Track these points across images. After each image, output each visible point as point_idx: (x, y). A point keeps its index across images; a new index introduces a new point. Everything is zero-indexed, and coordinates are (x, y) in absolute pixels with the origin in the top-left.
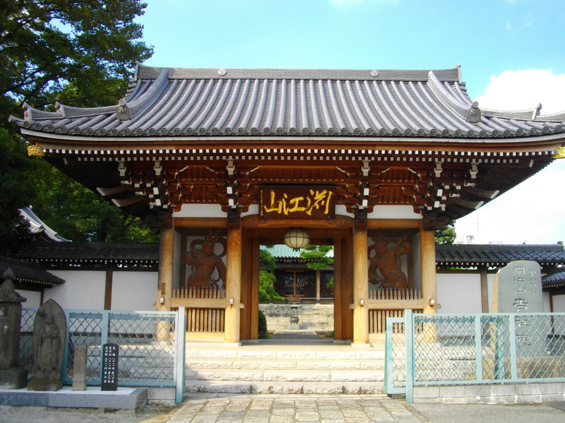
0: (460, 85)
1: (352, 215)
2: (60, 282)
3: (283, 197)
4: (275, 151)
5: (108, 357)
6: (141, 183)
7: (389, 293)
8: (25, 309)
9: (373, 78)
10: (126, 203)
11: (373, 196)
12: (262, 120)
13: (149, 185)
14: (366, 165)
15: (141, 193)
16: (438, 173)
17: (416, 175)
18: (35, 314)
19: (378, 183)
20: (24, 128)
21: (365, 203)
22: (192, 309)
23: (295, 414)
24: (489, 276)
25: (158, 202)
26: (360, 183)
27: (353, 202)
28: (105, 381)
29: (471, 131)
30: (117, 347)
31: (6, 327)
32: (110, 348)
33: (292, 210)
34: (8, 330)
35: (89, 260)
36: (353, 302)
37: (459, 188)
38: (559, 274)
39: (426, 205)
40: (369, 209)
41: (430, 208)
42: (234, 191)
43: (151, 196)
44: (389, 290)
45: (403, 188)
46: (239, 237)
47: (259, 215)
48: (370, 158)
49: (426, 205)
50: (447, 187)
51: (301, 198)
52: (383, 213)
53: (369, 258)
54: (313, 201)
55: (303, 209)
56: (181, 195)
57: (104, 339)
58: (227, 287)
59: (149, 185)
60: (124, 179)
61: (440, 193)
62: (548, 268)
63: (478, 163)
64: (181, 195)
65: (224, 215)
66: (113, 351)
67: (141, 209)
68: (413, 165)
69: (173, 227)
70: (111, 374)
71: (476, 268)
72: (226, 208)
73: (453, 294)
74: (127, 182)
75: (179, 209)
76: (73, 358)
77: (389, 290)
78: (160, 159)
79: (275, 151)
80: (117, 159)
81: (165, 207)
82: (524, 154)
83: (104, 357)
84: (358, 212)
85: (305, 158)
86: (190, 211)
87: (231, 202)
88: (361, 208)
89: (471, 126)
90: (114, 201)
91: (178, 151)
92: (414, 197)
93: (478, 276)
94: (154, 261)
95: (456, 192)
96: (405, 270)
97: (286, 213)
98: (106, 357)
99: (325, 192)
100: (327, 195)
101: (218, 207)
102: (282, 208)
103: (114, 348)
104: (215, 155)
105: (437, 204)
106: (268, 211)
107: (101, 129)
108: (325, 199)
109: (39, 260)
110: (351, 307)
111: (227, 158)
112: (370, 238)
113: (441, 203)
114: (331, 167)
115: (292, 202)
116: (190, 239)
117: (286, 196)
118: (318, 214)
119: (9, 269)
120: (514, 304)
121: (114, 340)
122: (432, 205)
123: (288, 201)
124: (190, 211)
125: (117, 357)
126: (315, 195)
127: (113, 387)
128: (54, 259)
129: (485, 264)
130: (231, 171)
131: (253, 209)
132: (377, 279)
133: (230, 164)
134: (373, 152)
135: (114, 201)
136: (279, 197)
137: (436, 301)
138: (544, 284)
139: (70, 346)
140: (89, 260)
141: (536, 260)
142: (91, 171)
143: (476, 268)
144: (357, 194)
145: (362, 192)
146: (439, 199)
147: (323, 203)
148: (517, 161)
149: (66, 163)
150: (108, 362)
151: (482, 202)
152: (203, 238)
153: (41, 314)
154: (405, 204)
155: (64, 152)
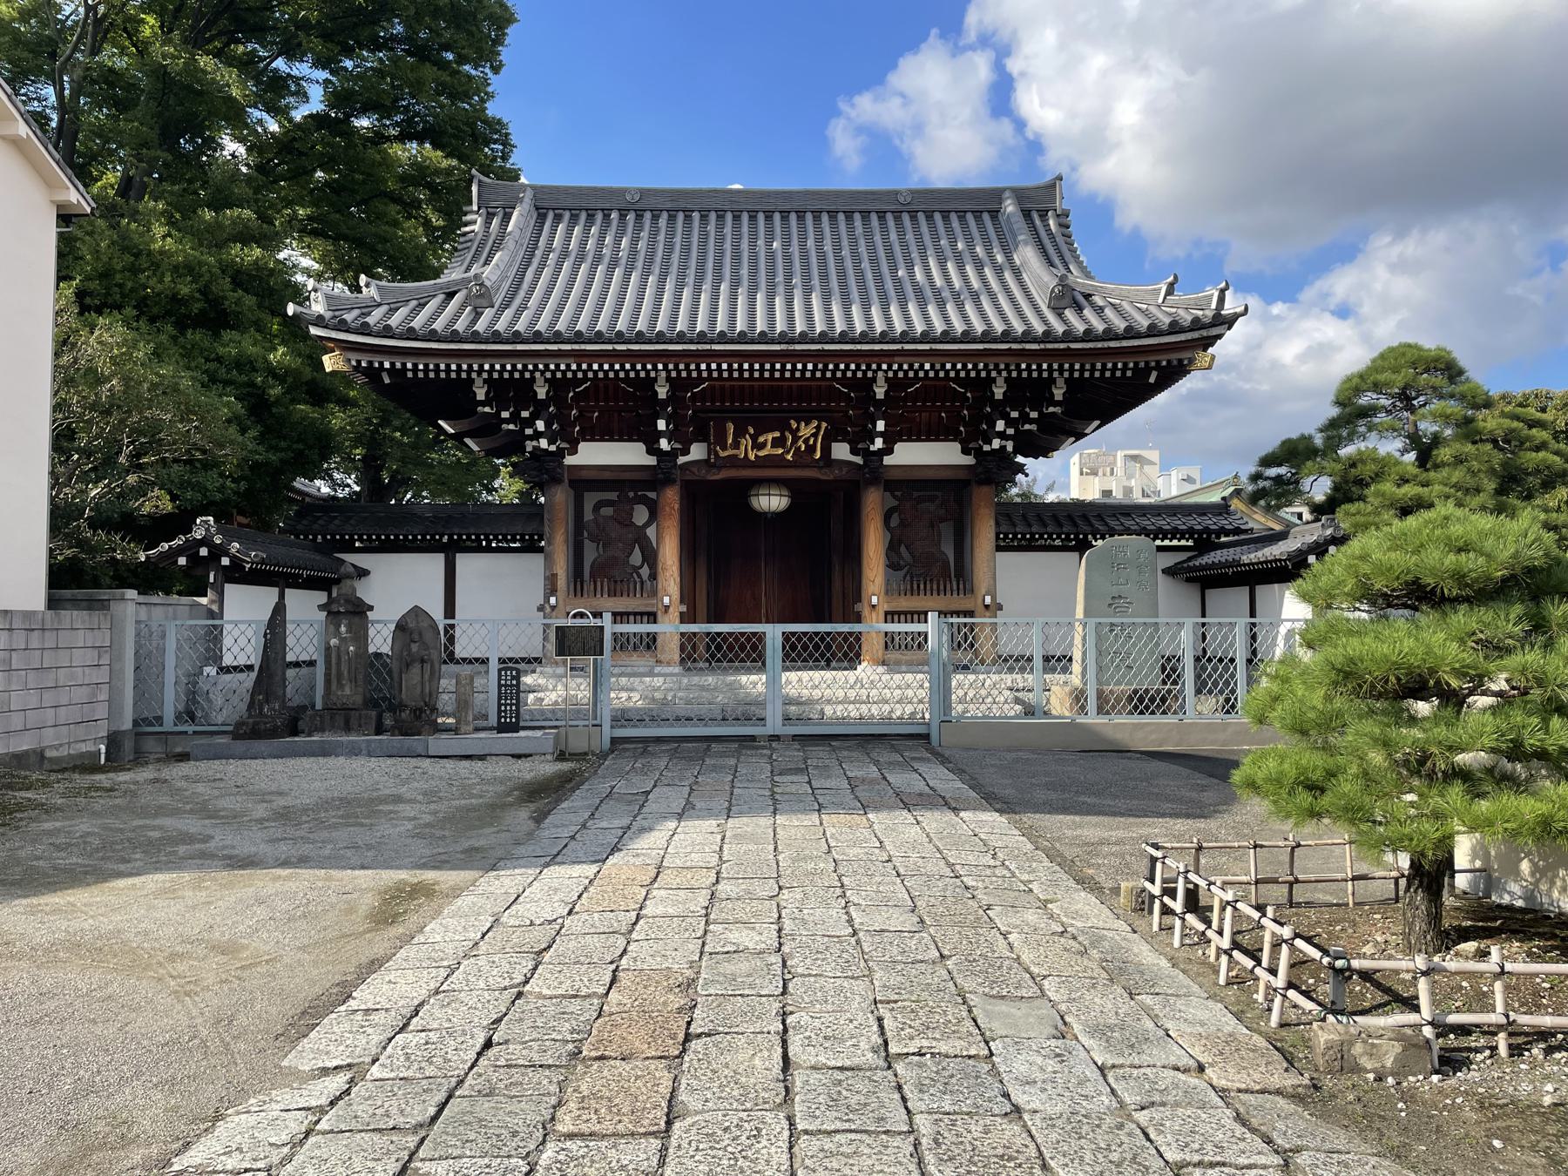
1: (858, 460)
3: (747, 431)
9: (900, 208)
12: (595, 318)
13: (525, 414)
15: (511, 427)
16: (999, 392)
21: (879, 443)
27: (861, 439)
33: (761, 453)
37: (1034, 415)
40: (888, 450)
43: (529, 431)
47: (707, 461)
50: (1015, 414)
51: (777, 434)
52: (908, 454)
54: (796, 439)
55: (780, 451)
58: (660, 578)
59: (525, 414)
60: (483, 404)
65: (651, 461)
66: (513, 678)
72: (652, 450)
73: (1020, 582)
74: (487, 409)
75: (574, 451)
84: (867, 454)
86: (593, 454)
88: (872, 448)
90: (468, 441)
95: (1031, 421)
97: (752, 458)
100: (818, 428)
101: (641, 447)
106: (723, 454)
108: (815, 435)
110: (857, 607)
115: (761, 439)
116: (590, 500)
117: (752, 431)
123: (754, 438)
124: (593, 454)
126: (798, 429)
127: (515, 728)
130: (662, 392)
131: (697, 452)
135: (468, 441)
136: (740, 433)
137: (994, 598)
152: (613, 496)
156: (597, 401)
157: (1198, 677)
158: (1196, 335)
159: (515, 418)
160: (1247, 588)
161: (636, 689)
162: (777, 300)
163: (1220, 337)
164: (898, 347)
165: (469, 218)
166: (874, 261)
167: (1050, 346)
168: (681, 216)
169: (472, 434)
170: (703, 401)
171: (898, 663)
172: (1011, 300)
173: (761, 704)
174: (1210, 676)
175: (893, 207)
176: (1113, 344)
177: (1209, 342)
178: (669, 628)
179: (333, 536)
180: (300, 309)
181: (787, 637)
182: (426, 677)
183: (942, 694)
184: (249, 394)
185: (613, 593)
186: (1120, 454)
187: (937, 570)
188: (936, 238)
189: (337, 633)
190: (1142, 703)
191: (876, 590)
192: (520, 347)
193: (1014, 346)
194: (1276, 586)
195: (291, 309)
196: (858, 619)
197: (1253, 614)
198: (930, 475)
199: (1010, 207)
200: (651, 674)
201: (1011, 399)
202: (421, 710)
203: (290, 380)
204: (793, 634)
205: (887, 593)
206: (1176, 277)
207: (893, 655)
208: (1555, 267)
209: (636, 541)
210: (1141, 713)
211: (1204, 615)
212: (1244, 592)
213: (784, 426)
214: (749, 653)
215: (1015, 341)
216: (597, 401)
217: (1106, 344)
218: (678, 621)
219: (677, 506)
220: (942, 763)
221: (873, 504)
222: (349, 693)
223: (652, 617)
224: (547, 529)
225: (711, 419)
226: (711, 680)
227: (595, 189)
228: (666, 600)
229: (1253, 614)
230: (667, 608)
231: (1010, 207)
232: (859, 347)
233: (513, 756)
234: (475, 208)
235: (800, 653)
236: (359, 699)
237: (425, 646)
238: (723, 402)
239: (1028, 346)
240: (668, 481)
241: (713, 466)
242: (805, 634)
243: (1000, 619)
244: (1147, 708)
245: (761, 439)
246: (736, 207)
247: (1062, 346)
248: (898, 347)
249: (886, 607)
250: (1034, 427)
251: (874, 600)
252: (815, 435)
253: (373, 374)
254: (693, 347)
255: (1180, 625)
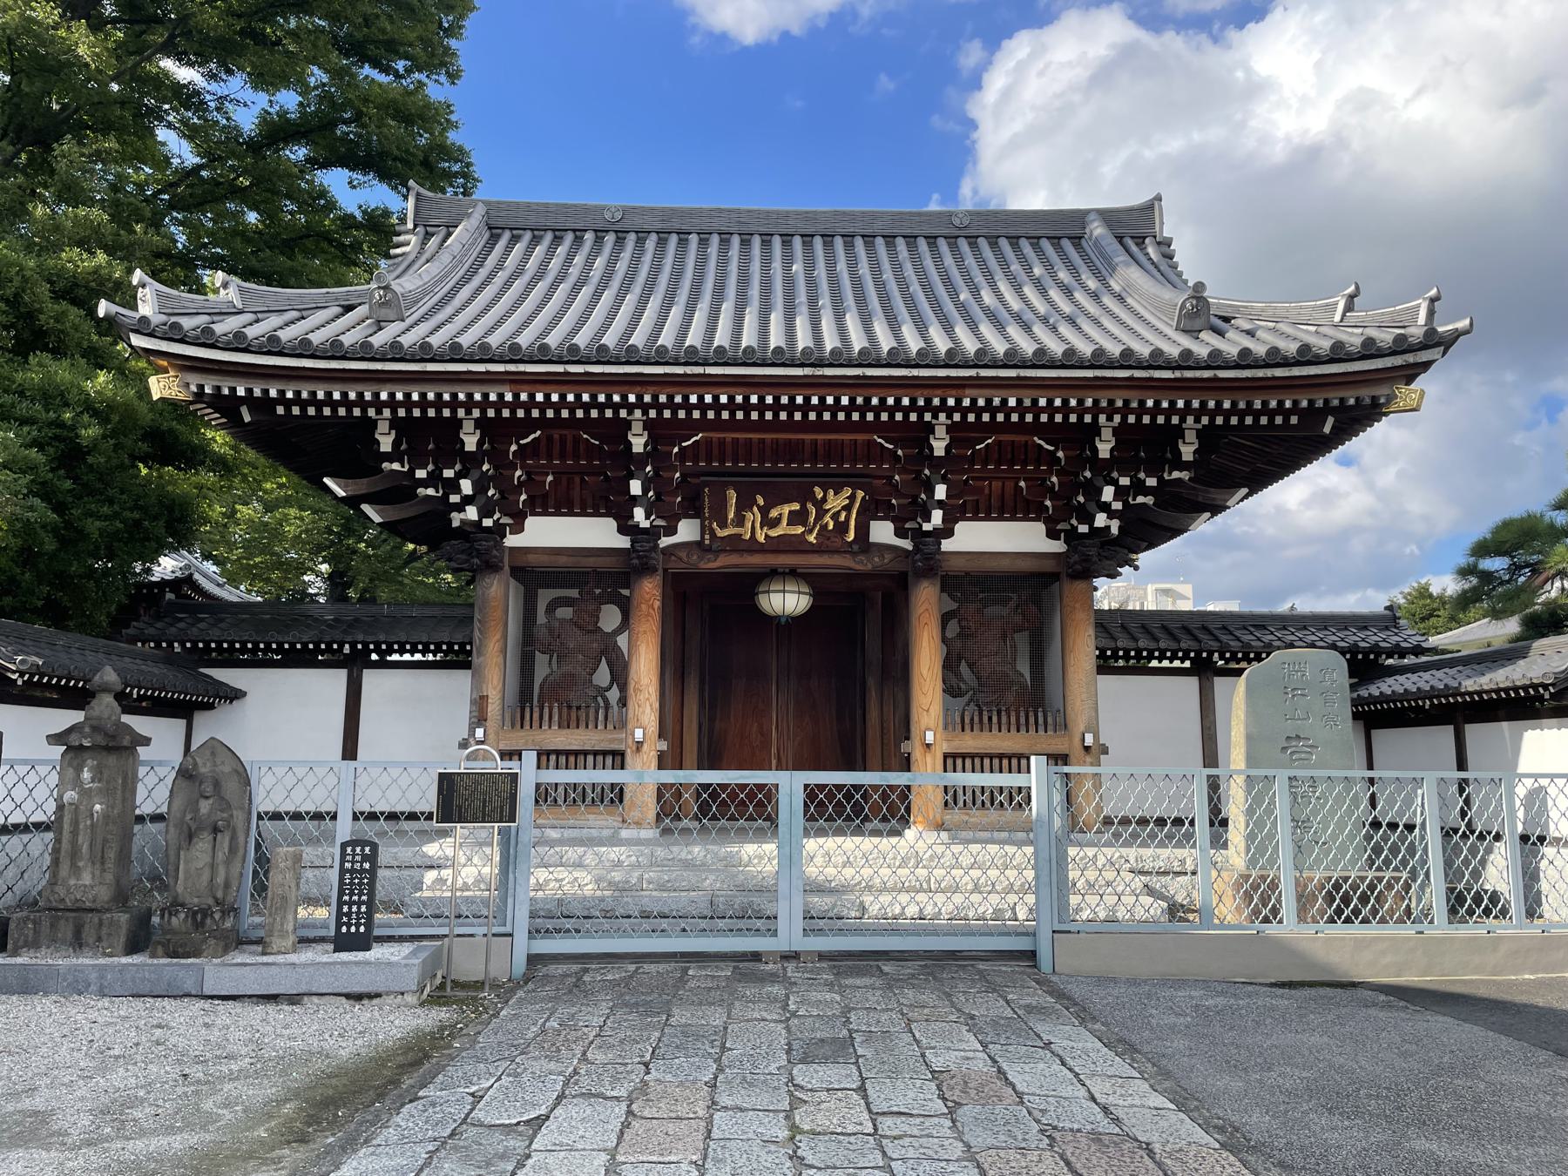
0: (1159, 243)
1: (906, 544)
2: (235, 695)
3: (755, 502)
4: (739, 399)
5: (352, 871)
6: (430, 467)
7: (990, 719)
8: (145, 763)
9: (958, 233)
10: (396, 513)
11: (953, 502)
13: (448, 473)
14: (940, 431)
15: (431, 492)
16: (1104, 449)
17: (1053, 453)
18: (174, 774)
19: (964, 472)
20: (137, 332)
21: (937, 517)
22: (548, 753)
23: (787, 997)
24: (1219, 682)
25: (472, 513)
26: (927, 472)
27: (907, 515)
28: (344, 929)
29: (1187, 353)
30: (374, 847)
31: (98, 807)
32: (358, 850)
33: (774, 533)
34: (106, 816)
35: (305, 645)
36: (908, 738)
37: (1151, 482)
38: (1390, 681)
39: (1074, 521)
40: (947, 532)
41: (1083, 529)
42: (645, 490)
43: (454, 499)
44: (990, 711)
45: (1022, 484)
46: (657, 593)
47: (699, 544)
48: (949, 417)
49: (1074, 521)
50: (1125, 481)
51: (796, 506)
52: (977, 538)
53: (944, 640)
54: (821, 513)
55: (800, 530)
56: (523, 497)
57: (344, 829)
58: (630, 704)
59: (448, 473)
60: (389, 457)
61: (1108, 493)
62: (1364, 666)
63: (1199, 426)
64: (523, 497)
65: (623, 542)
66: (365, 858)
67: (432, 527)
68: (1049, 431)
69: (507, 568)
70: (358, 913)
71: (1187, 664)
72: (626, 527)
73: (1134, 718)
74: (396, 466)
75: (518, 528)
76: (266, 873)
77: (990, 711)
78: (476, 413)
79: (739, 399)
80: (371, 412)
81: (488, 522)
82: (1311, 402)
83: (343, 871)
84: (918, 535)
85: (805, 416)
86: (545, 532)
87: (639, 514)
88: (927, 527)
89: (1186, 342)
90: (366, 508)
91: (516, 396)
92: (1048, 503)
93: (1193, 682)
94: (462, 645)
95: (1147, 491)
96: (1024, 668)
97: (761, 539)
98: (348, 871)
99: (848, 492)
100: (852, 498)
101: (611, 523)
102: (753, 527)
103: (367, 850)
104: (601, 408)
105: (1101, 520)
106: (721, 533)
107: (336, 343)
108: (848, 508)
109: (183, 645)
110: (905, 747)
111: (630, 413)
112: (945, 595)
113: (1110, 517)
114: (860, 437)
115: (774, 513)
116: (545, 597)
117: (761, 501)
118: (831, 541)
119: (108, 669)
120: (1284, 749)
121: (369, 829)
122: (1090, 520)
123: (764, 511)
124: (545, 532)
125: (374, 867)
126: (824, 500)
127: (362, 942)
128: (219, 644)
129: (1211, 654)
130: (638, 443)
131: (687, 531)
132: (963, 686)
133: (637, 427)
134: (959, 401)
135: (366, 508)
136: (745, 504)
137: (1096, 738)
138: (1356, 702)
139: (258, 846)
140: (305, 645)
141: (1333, 647)
142: (307, 436)
143: (1187, 664)
144: (918, 496)
145: (931, 492)
146: (1105, 507)
147: (842, 518)
148: (1294, 420)
149: (247, 418)
150: (351, 884)
151: (1208, 515)
152: (574, 593)
153: (186, 774)
154: (1026, 519)
155: (241, 392)
156: (550, 458)
157: (1448, 863)
158: (1398, 361)
159: (434, 479)
160: (1451, 728)
161: (576, 866)
162: (798, 321)
163: (1426, 365)
164: (971, 373)
165: (401, 238)
166: (927, 287)
167: (1189, 374)
168: (674, 239)
169: (371, 499)
170: (696, 460)
171: (965, 826)
172: (1129, 322)
173: (767, 890)
174: (1466, 862)
175: (946, 232)
176: (1279, 372)
177: (1410, 373)
178: (643, 776)
179: (195, 644)
180: (115, 309)
181: (811, 792)
182: (220, 856)
183: (1054, 879)
184: (56, 438)
185: (565, 724)
186: (1150, 588)
187: (1012, 693)
188: (1004, 265)
189: (77, 783)
190: (1346, 902)
191: (932, 725)
192: (431, 367)
193: (1138, 374)
194: (1505, 724)
195: (103, 308)
196: (906, 764)
197: (1462, 765)
198: (1005, 565)
199: (1097, 229)
200: (614, 841)
201: (1121, 460)
202: (206, 912)
203: (115, 418)
204: (821, 787)
205: (946, 728)
206: (1357, 288)
207: (956, 815)
208: (1552, 419)
209: (602, 653)
210: (1348, 921)
211: (1370, 767)
212: (1446, 734)
213: (805, 496)
214: (755, 810)
215: (1140, 366)
216: (550, 458)
217: (1269, 373)
218: (654, 763)
219: (657, 604)
220: (1083, 1022)
221: (926, 602)
222: (88, 883)
223: (617, 758)
224: (477, 633)
225: (707, 484)
226: (697, 850)
227: (565, 206)
228: (639, 734)
229: (1462, 765)
230: (639, 745)
231: (1097, 229)
232: (915, 372)
233: (348, 996)
234: (410, 225)
235: (828, 811)
236: (104, 894)
237: (225, 805)
238: (722, 462)
239: (1158, 374)
240: (646, 569)
241: (709, 550)
242: (839, 787)
243: (1106, 767)
244: (1356, 912)
245: (774, 513)
246: (745, 229)
247: (1207, 374)
248: (971, 373)
249: (946, 748)
250: (1149, 500)
251: (930, 737)
252: (848, 508)
253: (226, 406)
254: (679, 370)
255: (1418, 782)
